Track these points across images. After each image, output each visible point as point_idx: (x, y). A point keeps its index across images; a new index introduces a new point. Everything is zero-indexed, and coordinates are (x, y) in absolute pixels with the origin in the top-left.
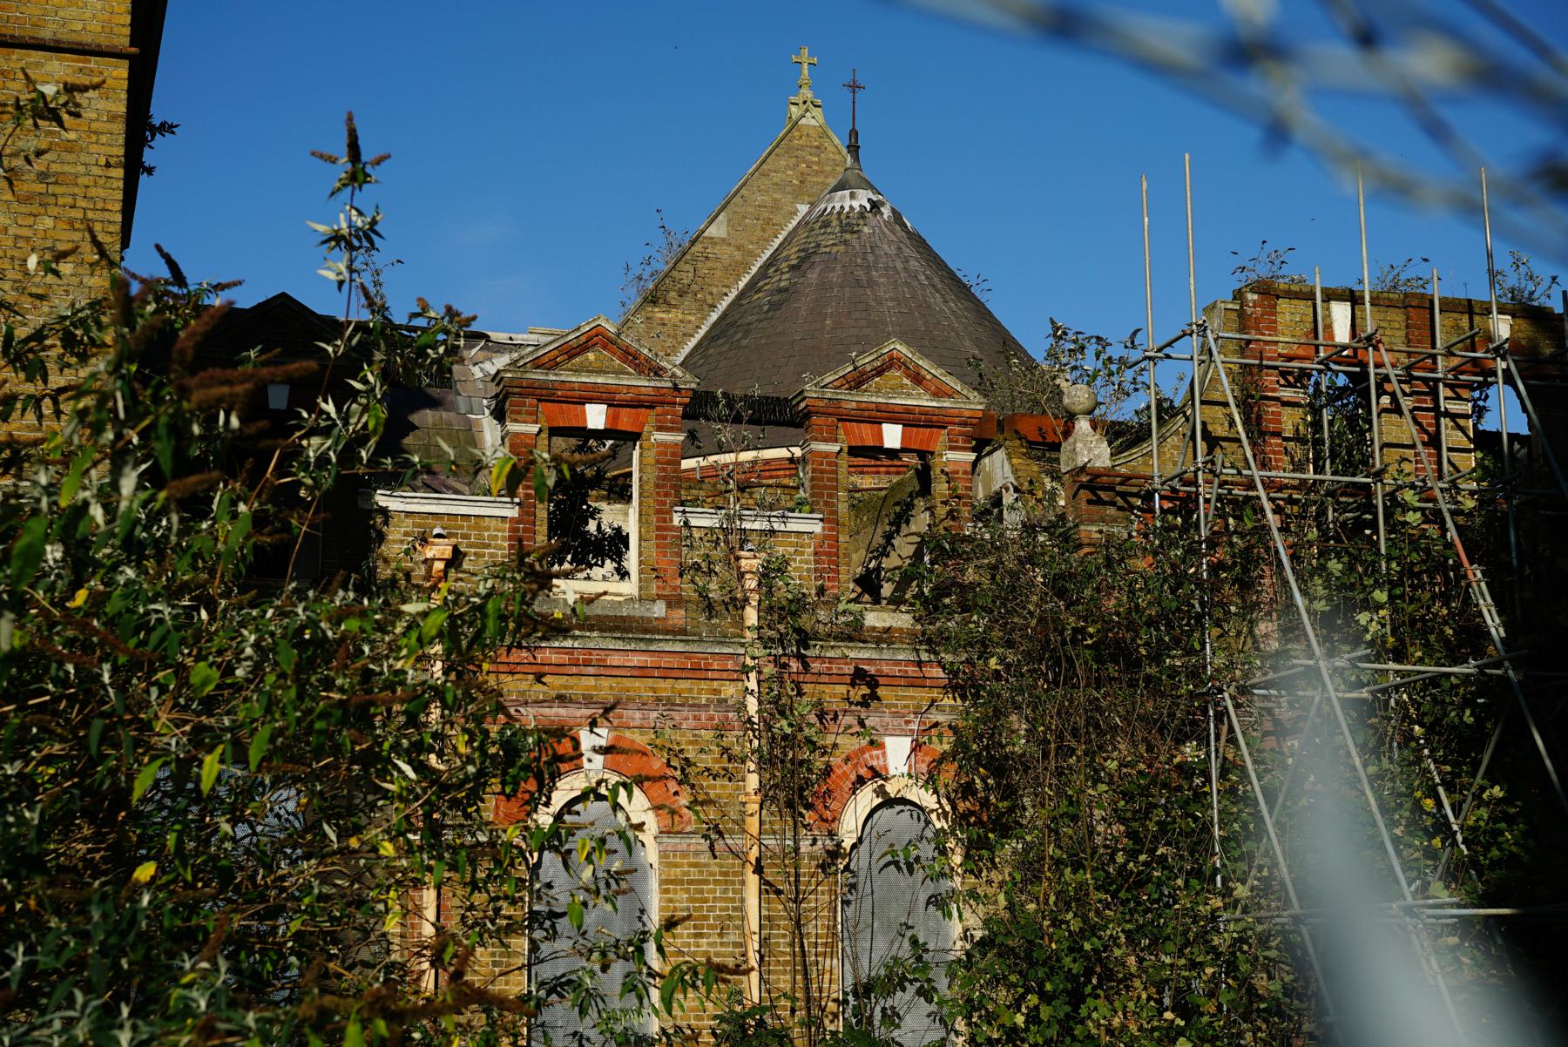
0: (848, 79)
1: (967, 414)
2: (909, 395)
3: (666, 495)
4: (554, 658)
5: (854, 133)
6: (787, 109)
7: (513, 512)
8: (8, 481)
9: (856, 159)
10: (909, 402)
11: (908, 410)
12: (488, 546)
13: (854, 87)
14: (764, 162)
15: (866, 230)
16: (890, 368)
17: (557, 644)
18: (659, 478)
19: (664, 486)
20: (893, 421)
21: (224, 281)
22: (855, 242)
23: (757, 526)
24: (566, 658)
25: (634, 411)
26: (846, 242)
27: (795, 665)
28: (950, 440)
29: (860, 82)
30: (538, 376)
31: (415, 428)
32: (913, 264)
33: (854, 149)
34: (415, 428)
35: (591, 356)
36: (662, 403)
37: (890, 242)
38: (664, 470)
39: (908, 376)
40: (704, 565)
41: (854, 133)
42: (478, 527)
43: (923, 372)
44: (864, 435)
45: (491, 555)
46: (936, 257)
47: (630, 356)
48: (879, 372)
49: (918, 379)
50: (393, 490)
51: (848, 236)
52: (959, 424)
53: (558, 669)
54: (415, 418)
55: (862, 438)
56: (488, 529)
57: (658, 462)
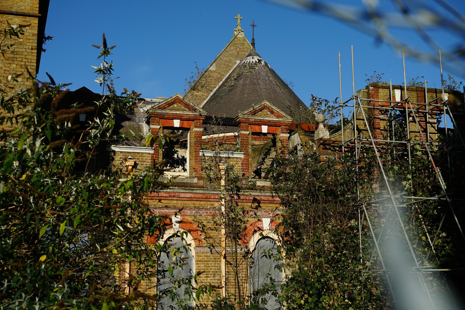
0: (251, 23)
1: (287, 122)
2: (269, 117)
3: (198, 146)
4: (164, 195)
5: (253, 39)
6: (234, 32)
7: (152, 152)
8: (2, 143)
9: (254, 47)
10: (270, 119)
11: (269, 121)
12: (145, 162)
13: (253, 26)
14: (227, 48)
15: (257, 68)
16: (264, 109)
17: (165, 191)
18: (195, 141)
19: (197, 144)
20: (265, 125)
21: (66, 83)
22: (253, 72)
23: (224, 156)
24: (168, 195)
25: (188, 122)
26: (251, 72)
27: (236, 197)
28: (282, 130)
29: (255, 24)
30: (159, 111)
31: (123, 127)
32: (271, 78)
33: (253, 44)
34: (123, 127)
35: (175, 105)
36: (196, 119)
37: (264, 72)
38: (197, 139)
39: (269, 111)
40: (209, 167)
41: (253, 39)
42: (142, 156)
43: (274, 110)
44: (256, 129)
45: (146, 164)
46: (278, 76)
47: (187, 106)
48: (261, 110)
49: (272, 112)
50: (117, 145)
51: (251, 70)
52: (285, 126)
53: (166, 198)
54: (123, 124)
55: (256, 130)
56: (145, 157)
57: (195, 137)
